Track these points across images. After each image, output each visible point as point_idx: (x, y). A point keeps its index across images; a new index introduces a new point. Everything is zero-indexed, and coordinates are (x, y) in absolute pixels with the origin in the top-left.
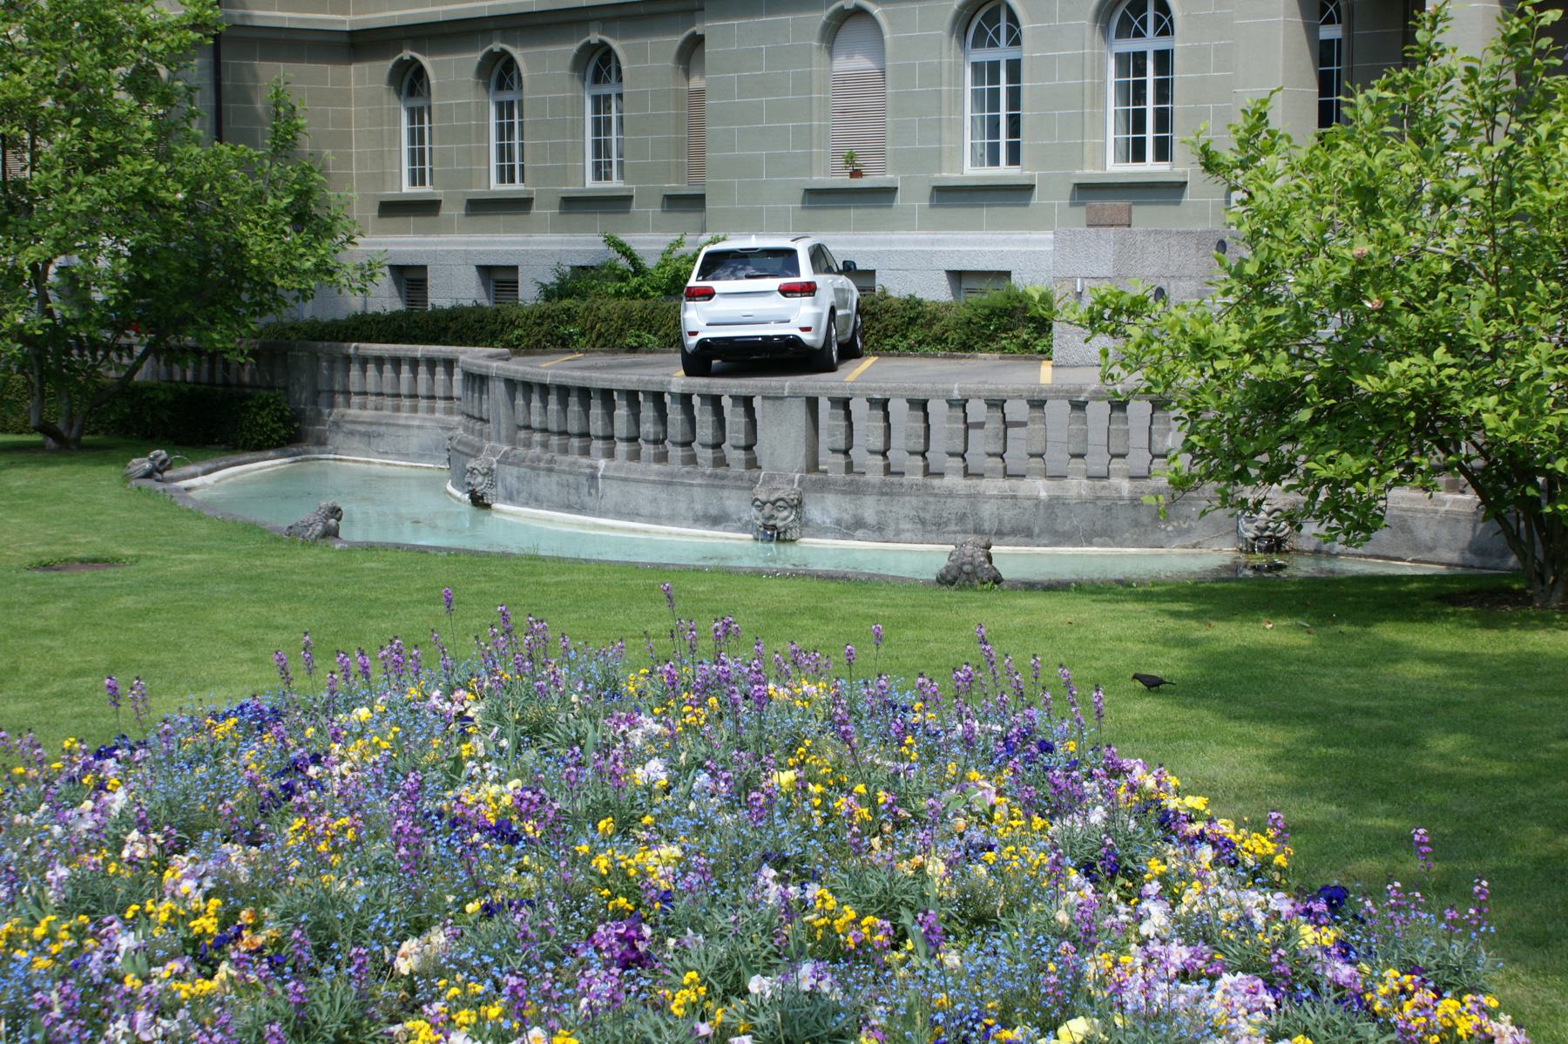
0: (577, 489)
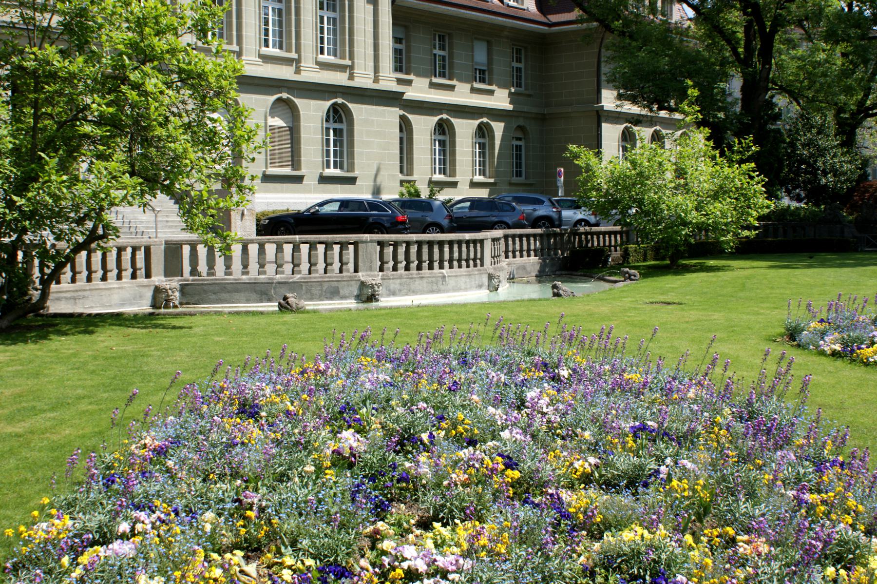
0: (437, 284)
